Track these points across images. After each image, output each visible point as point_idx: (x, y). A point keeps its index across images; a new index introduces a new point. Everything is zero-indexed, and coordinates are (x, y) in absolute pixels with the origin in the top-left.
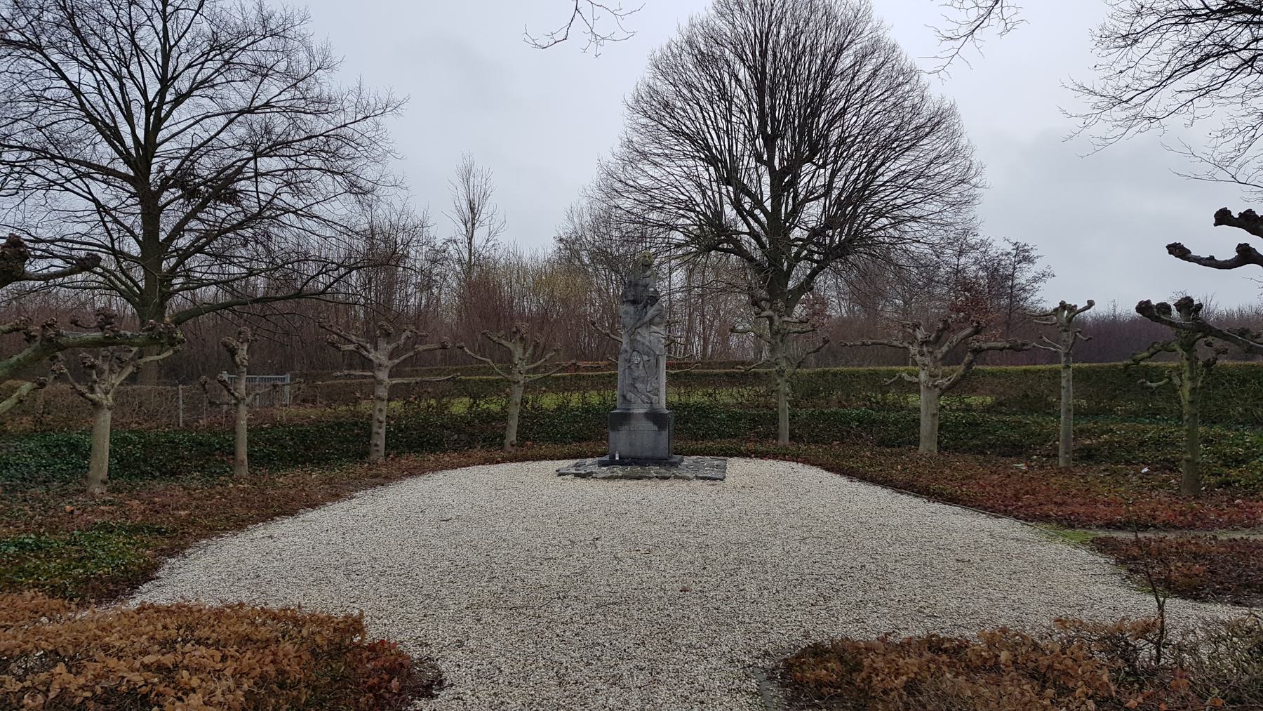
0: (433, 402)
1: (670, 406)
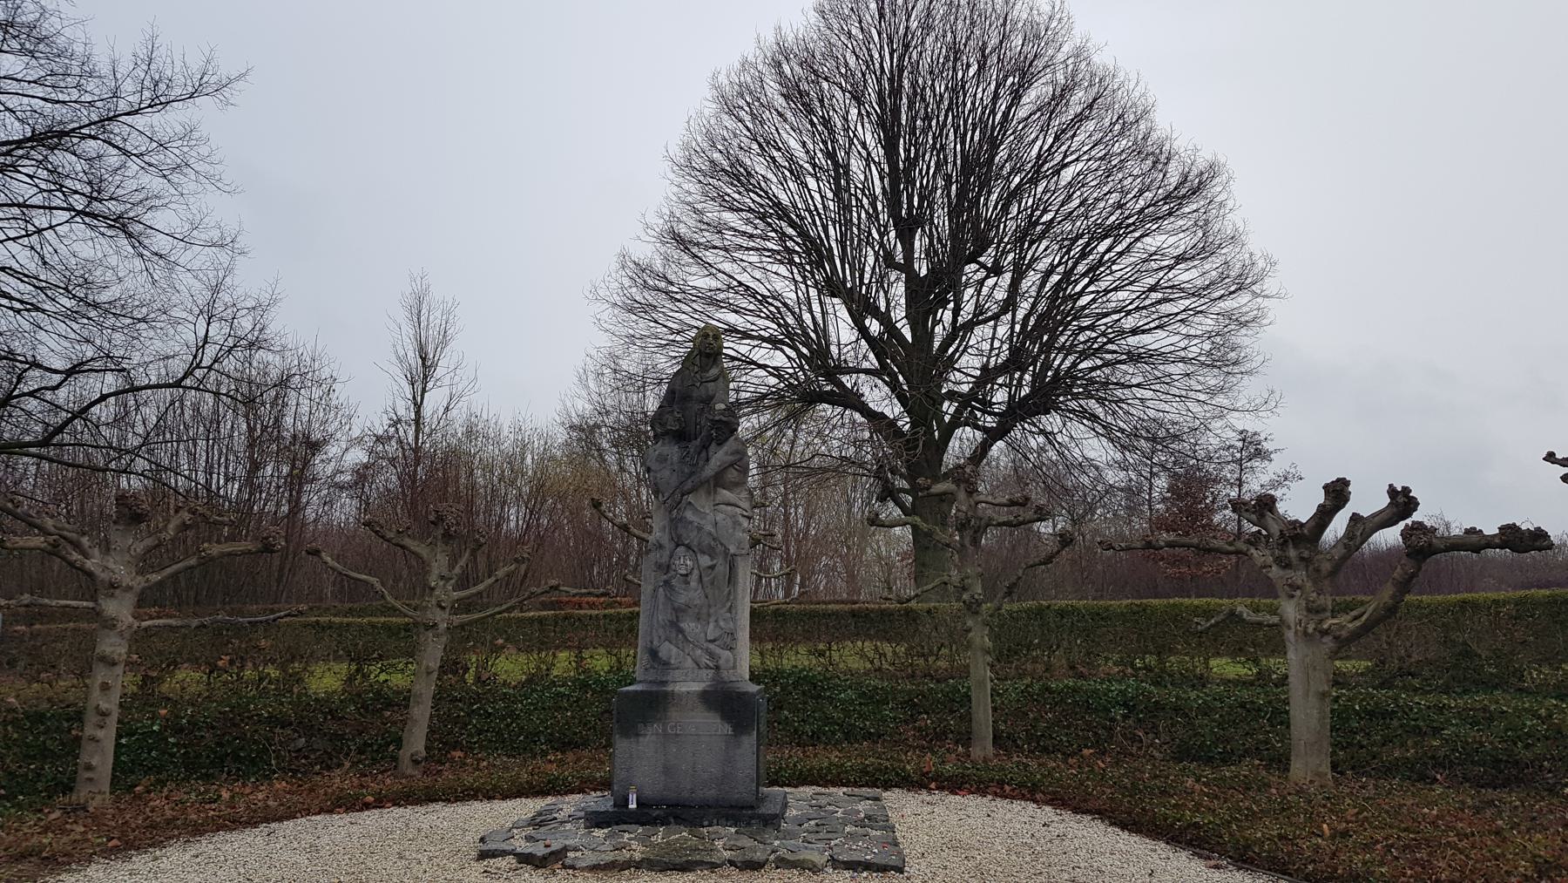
0: (273, 672)
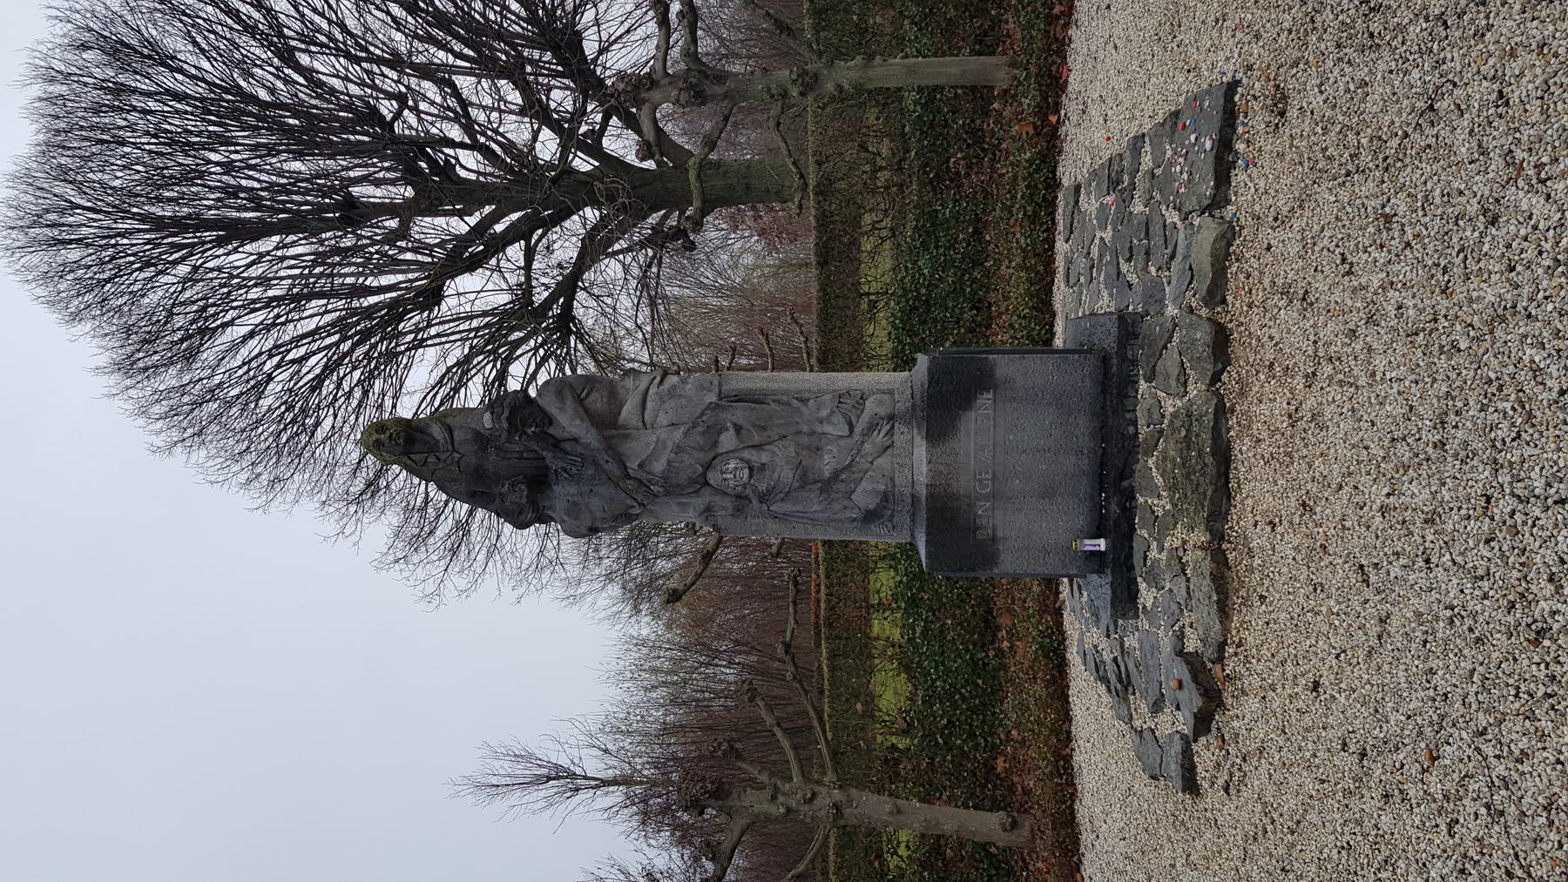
1: (903, 362)
